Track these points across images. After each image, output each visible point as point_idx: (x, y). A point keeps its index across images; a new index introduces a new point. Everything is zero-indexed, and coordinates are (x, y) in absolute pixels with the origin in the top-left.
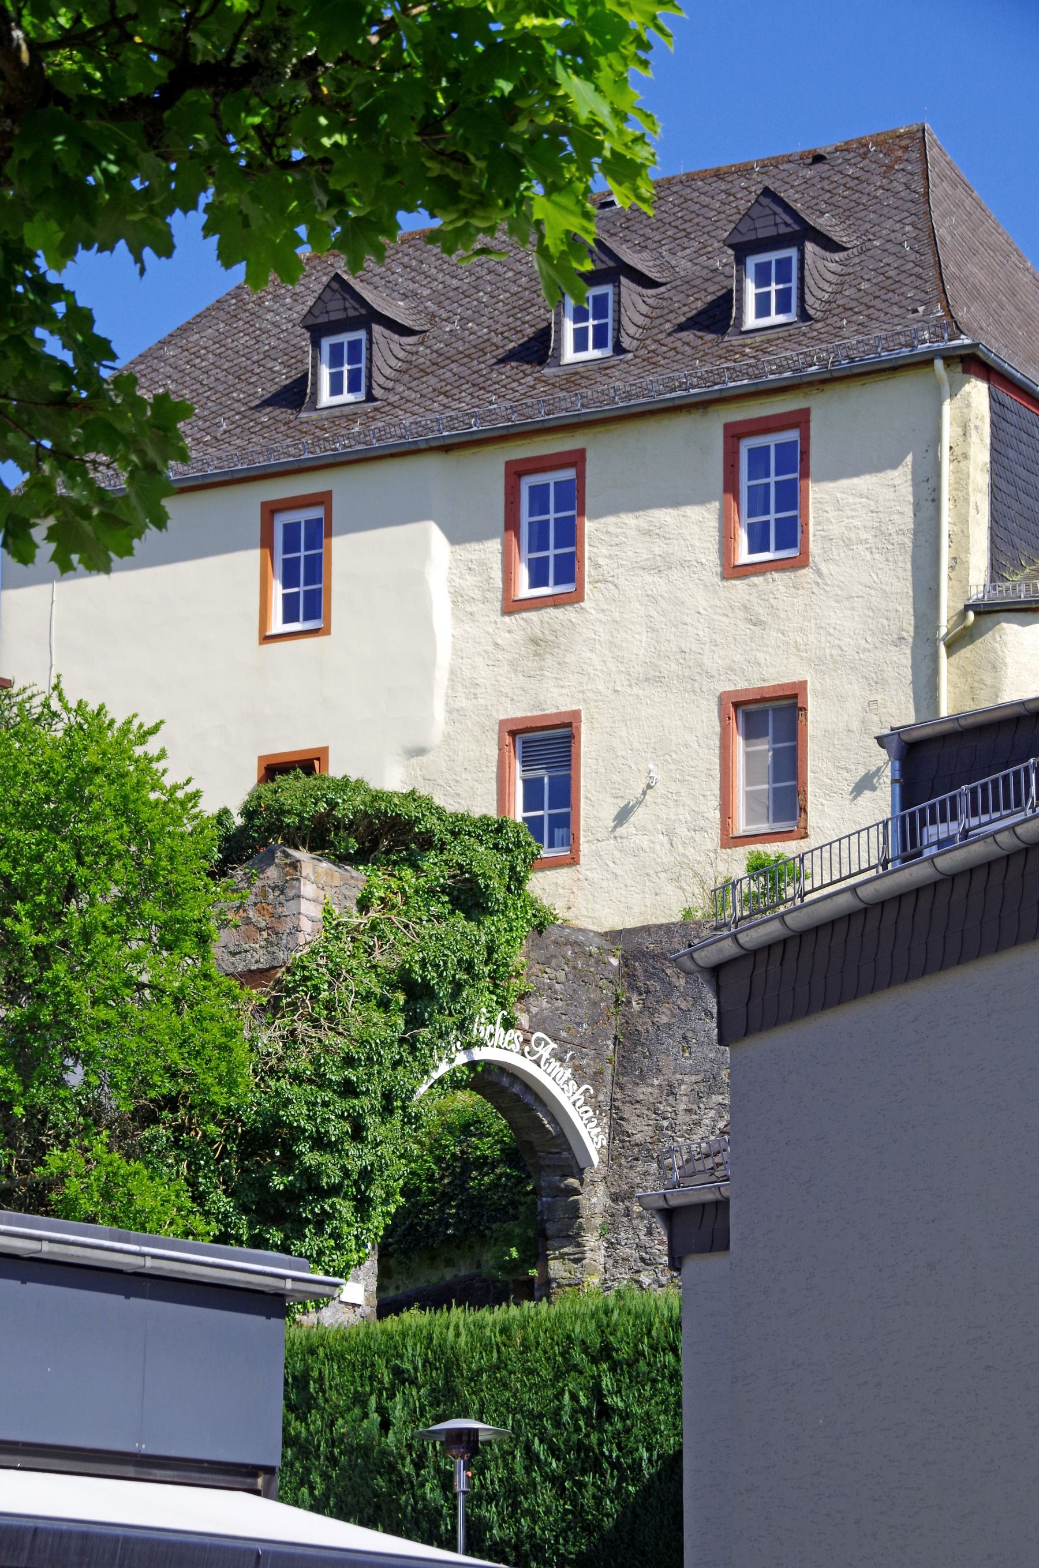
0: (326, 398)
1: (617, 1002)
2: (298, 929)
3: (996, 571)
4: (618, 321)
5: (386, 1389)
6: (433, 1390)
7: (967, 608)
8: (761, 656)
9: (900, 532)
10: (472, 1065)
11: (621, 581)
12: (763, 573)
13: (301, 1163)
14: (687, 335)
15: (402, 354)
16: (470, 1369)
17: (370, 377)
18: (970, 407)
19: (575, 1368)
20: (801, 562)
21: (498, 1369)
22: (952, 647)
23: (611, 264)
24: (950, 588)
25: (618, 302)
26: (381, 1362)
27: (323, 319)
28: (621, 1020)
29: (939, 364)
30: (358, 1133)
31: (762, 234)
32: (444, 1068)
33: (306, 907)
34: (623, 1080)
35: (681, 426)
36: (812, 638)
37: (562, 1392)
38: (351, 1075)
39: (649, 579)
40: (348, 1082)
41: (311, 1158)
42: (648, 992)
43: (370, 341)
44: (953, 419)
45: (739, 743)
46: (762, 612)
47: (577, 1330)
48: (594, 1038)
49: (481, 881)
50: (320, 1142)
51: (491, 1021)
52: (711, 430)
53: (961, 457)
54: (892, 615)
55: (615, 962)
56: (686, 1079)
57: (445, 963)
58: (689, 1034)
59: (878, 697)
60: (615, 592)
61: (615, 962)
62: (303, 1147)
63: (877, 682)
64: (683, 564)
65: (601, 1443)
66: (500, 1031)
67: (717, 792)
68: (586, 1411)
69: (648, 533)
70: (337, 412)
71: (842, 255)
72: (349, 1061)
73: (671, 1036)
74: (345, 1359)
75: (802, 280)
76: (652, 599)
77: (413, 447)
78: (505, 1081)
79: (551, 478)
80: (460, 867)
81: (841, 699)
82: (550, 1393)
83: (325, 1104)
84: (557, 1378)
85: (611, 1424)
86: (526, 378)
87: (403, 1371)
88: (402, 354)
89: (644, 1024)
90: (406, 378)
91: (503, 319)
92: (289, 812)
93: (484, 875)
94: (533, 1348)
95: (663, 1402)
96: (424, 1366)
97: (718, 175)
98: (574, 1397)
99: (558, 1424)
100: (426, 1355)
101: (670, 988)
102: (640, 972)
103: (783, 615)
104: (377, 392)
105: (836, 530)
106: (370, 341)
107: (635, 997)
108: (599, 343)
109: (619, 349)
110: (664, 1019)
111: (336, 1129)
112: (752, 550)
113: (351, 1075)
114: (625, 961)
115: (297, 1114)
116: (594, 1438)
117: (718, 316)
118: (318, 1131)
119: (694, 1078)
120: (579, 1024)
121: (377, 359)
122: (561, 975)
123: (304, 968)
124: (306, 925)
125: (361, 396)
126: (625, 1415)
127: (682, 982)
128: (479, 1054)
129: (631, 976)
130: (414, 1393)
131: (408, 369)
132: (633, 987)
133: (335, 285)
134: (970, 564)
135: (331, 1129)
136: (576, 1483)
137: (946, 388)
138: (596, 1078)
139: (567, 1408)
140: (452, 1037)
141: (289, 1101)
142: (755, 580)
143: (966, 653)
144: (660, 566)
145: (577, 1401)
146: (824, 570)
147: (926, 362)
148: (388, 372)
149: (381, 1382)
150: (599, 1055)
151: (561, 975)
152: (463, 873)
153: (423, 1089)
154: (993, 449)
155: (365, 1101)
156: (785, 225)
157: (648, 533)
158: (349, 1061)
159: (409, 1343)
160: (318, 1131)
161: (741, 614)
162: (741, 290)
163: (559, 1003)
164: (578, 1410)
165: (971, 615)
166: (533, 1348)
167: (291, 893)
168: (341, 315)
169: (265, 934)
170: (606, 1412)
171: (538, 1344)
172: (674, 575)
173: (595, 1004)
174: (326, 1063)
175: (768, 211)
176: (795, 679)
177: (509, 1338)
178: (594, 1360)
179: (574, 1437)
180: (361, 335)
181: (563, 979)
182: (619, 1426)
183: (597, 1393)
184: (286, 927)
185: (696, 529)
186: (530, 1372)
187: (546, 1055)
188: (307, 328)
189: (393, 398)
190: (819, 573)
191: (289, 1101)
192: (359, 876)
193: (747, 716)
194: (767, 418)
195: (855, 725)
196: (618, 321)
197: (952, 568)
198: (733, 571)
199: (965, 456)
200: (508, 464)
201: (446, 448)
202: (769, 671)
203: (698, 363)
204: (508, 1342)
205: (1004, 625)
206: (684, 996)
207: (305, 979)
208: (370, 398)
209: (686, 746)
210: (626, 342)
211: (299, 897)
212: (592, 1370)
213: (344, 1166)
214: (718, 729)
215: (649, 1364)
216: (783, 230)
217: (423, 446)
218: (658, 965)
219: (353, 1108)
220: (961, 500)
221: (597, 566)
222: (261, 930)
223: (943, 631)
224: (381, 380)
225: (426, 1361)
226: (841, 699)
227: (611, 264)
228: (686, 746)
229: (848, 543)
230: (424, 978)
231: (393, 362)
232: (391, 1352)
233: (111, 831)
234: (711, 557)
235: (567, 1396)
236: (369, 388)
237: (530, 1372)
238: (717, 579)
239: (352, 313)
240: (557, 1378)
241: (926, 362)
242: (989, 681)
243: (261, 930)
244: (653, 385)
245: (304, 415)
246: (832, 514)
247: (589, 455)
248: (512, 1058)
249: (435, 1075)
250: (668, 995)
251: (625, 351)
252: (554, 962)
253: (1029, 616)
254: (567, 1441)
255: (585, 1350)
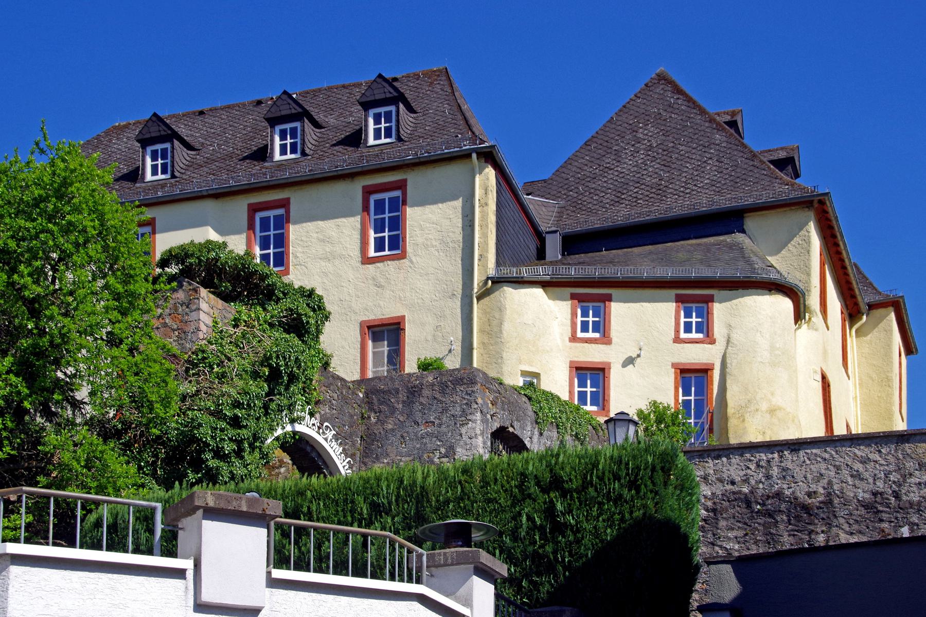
0: (149, 177)
1: (363, 418)
2: (198, 329)
3: (498, 264)
4: (303, 140)
5: (365, 519)
6: (405, 518)
7: (488, 278)
8: (382, 303)
9: (453, 242)
10: (295, 433)
11: (309, 265)
12: (383, 261)
13: (207, 466)
14: (336, 148)
15: (188, 158)
16: (438, 501)
17: (173, 166)
18: (486, 180)
19: (529, 496)
20: (403, 256)
21: (462, 499)
22: (479, 298)
23: (300, 110)
24: (479, 270)
25: (303, 130)
26: (360, 499)
27: (148, 136)
28: (363, 428)
29: (474, 156)
30: (239, 453)
31: (378, 97)
32: (279, 432)
33: (202, 316)
34: (366, 460)
35: (340, 188)
36: (408, 294)
37: (520, 514)
38: (238, 412)
39: (324, 264)
40: (236, 417)
41: (213, 463)
42: (380, 412)
43: (173, 148)
44: (480, 185)
45: (370, 343)
46: (382, 281)
47: (531, 468)
48: (351, 435)
49: (304, 319)
50: (219, 454)
51: (303, 410)
52: (356, 188)
53: (484, 205)
54: (448, 283)
55: (361, 395)
56: (403, 459)
57: (290, 357)
58: (405, 435)
59: (442, 324)
60: (306, 270)
61: (361, 395)
62: (208, 456)
63: (442, 317)
64: (341, 256)
65: (555, 552)
66: (308, 417)
67: (359, 371)
68: (541, 528)
69: (323, 241)
70: (156, 183)
71: (415, 115)
72: (237, 405)
73: (394, 436)
74: (329, 498)
75: (398, 121)
76: (325, 274)
77: (200, 194)
78: (309, 449)
79: (271, 214)
80: (291, 310)
81: (423, 324)
82: (508, 515)
83: (222, 430)
84: (513, 505)
85: (564, 537)
86: (256, 167)
87: (379, 505)
88: (188, 158)
89: (377, 430)
90: (191, 169)
91: (240, 144)
92: (192, 255)
93: (306, 315)
94: (492, 483)
95: (608, 520)
96: (397, 501)
97: (344, 87)
98: (530, 518)
99: (515, 537)
100: (399, 493)
101: (393, 410)
102: (375, 401)
103: (393, 282)
104: (177, 174)
105: (420, 240)
106: (173, 148)
107: (373, 415)
108: (293, 151)
109: (304, 154)
110: (390, 426)
111: (228, 447)
112: (375, 252)
113: (238, 412)
114: (367, 394)
115: (205, 433)
116: (549, 548)
117: (355, 139)
118: (217, 447)
119: (407, 458)
120: (344, 425)
121: (177, 158)
122: (335, 396)
123: (203, 352)
124: (203, 327)
125: (168, 176)
126: (577, 530)
127: (401, 406)
128: (299, 428)
129: (370, 403)
130: (389, 520)
131: (191, 165)
132: (371, 409)
133: (154, 119)
134: (487, 262)
135: (226, 446)
136: (531, 582)
137: (477, 169)
138: (352, 456)
139: (524, 526)
140: (284, 413)
141: (200, 425)
142: (378, 265)
143: (486, 301)
144: (328, 258)
145: (534, 521)
146: (414, 259)
147: (467, 156)
148: (182, 165)
149: (361, 514)
150: (354, 445)
151: (335, 396)
152: (292, 314)
153: (269, 441)
154: (497, 204)
155: (244, 431)
156: (389, 92)
157: (323, 241)
158: (237, 405)
159: (384, 485)
160: (217, 447)
161: (371, 282)
162: (366, 126)
163: (334, 412)
164: (533, 527)
165: (490, 282)
166: (492, 483)
167: (194, 307)
168: (158, 134)
169: (177, 333)
170: (559, 528)
171: (496, 480)
172: (337, 262)
173: (352, 416)
174: (223, 404)
175: (380, 86)
176: (399, 314)
177: (471, 476)
178: (545, 491)
179: (530, 549)
180: (167, 145)
181: (336, 398)
182: (571, 538)
183: (549, 511)
184: (192, 328)
185: (348, 239)
186: (489, 501)
187: (330, 437)
188: (138, 141)
189: (184, 177)
190: (411, 262)
191: (200, 425)
192: (233, 309)
193: (373, 333)
194: (385, 183)
195: (430, 338)
196: (303, 140)
197: (479, 260)
198: (367, 261)
199: (486, 204)
200: (249, 205)
201: (217, 196)
202: (386, 311)
203: (346, 158)
204: (470, 480)
205: (505, 288)
206: (402, 413)
207: (204, 358)
208: (173, 176)
209: (343, 347)
210: (307, 151)
211: (199, 309)
212: (542, 498)
213: (231, 472)
214: (359, 339)
215: (596, 490)
216: (388, 95)
217: (205, 193)
218: (386, 397)
219: (239, 434)
220: (484, 226)
221: (296, 257)
222: (174, 330)
223: (475, 290)
224: (179, 169)
225: (398, 496)
226: (423, 324)
227: (300, 110)
228: (343, 347)
229: (426, 247)
230: (277, 364)
231: (184, 162)
232: (368, 492)
233: (90, 223)
234: (356, 253)
235: (524, 519)
236: (173, 172)
237: (489, 501)
238: (359, 264)
239: (163, 133)
240: (513, 505)
241: (467, 156)
242: (497, 316)
243: (174, 330)
244: (326, 167)
245: (138, 185)
246: (418, 232)
247: (292, 201)
248: (313, 433)
249: (276, 435)
250: (393, 413)
251: (307, 155)
252: (332, 388)
253: (517, 285)
254: (524, 552)
255: (538, 484)
